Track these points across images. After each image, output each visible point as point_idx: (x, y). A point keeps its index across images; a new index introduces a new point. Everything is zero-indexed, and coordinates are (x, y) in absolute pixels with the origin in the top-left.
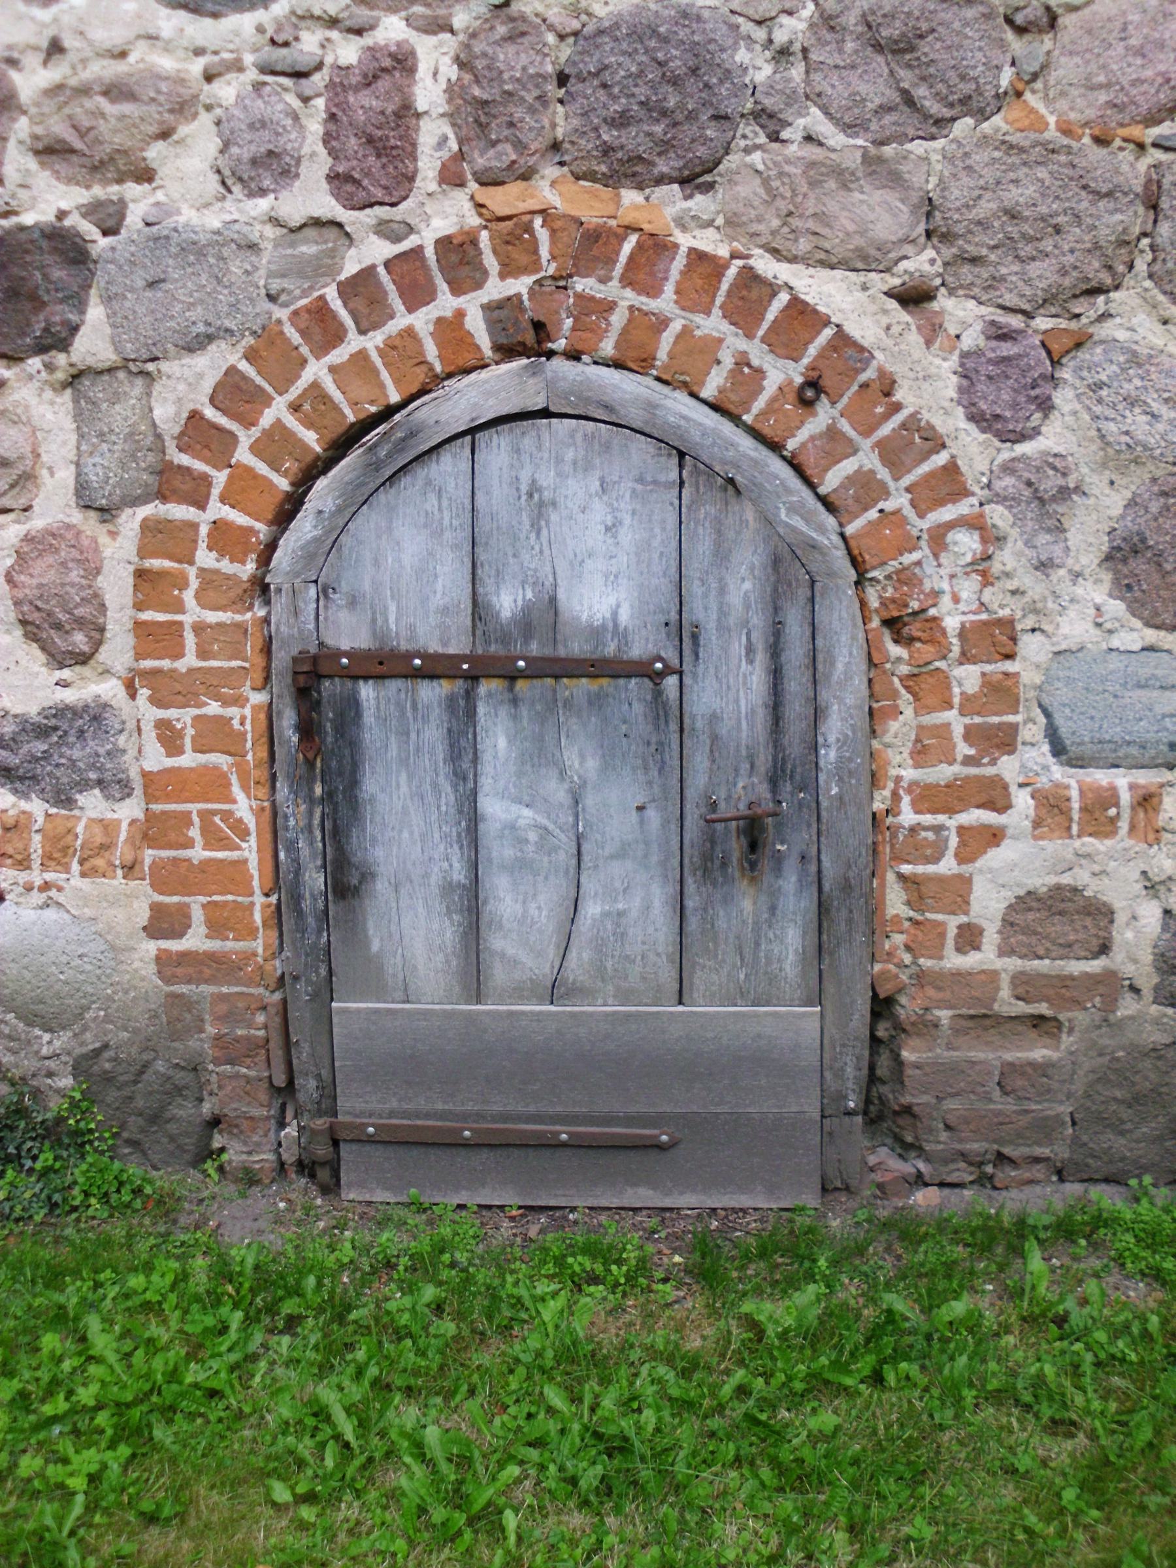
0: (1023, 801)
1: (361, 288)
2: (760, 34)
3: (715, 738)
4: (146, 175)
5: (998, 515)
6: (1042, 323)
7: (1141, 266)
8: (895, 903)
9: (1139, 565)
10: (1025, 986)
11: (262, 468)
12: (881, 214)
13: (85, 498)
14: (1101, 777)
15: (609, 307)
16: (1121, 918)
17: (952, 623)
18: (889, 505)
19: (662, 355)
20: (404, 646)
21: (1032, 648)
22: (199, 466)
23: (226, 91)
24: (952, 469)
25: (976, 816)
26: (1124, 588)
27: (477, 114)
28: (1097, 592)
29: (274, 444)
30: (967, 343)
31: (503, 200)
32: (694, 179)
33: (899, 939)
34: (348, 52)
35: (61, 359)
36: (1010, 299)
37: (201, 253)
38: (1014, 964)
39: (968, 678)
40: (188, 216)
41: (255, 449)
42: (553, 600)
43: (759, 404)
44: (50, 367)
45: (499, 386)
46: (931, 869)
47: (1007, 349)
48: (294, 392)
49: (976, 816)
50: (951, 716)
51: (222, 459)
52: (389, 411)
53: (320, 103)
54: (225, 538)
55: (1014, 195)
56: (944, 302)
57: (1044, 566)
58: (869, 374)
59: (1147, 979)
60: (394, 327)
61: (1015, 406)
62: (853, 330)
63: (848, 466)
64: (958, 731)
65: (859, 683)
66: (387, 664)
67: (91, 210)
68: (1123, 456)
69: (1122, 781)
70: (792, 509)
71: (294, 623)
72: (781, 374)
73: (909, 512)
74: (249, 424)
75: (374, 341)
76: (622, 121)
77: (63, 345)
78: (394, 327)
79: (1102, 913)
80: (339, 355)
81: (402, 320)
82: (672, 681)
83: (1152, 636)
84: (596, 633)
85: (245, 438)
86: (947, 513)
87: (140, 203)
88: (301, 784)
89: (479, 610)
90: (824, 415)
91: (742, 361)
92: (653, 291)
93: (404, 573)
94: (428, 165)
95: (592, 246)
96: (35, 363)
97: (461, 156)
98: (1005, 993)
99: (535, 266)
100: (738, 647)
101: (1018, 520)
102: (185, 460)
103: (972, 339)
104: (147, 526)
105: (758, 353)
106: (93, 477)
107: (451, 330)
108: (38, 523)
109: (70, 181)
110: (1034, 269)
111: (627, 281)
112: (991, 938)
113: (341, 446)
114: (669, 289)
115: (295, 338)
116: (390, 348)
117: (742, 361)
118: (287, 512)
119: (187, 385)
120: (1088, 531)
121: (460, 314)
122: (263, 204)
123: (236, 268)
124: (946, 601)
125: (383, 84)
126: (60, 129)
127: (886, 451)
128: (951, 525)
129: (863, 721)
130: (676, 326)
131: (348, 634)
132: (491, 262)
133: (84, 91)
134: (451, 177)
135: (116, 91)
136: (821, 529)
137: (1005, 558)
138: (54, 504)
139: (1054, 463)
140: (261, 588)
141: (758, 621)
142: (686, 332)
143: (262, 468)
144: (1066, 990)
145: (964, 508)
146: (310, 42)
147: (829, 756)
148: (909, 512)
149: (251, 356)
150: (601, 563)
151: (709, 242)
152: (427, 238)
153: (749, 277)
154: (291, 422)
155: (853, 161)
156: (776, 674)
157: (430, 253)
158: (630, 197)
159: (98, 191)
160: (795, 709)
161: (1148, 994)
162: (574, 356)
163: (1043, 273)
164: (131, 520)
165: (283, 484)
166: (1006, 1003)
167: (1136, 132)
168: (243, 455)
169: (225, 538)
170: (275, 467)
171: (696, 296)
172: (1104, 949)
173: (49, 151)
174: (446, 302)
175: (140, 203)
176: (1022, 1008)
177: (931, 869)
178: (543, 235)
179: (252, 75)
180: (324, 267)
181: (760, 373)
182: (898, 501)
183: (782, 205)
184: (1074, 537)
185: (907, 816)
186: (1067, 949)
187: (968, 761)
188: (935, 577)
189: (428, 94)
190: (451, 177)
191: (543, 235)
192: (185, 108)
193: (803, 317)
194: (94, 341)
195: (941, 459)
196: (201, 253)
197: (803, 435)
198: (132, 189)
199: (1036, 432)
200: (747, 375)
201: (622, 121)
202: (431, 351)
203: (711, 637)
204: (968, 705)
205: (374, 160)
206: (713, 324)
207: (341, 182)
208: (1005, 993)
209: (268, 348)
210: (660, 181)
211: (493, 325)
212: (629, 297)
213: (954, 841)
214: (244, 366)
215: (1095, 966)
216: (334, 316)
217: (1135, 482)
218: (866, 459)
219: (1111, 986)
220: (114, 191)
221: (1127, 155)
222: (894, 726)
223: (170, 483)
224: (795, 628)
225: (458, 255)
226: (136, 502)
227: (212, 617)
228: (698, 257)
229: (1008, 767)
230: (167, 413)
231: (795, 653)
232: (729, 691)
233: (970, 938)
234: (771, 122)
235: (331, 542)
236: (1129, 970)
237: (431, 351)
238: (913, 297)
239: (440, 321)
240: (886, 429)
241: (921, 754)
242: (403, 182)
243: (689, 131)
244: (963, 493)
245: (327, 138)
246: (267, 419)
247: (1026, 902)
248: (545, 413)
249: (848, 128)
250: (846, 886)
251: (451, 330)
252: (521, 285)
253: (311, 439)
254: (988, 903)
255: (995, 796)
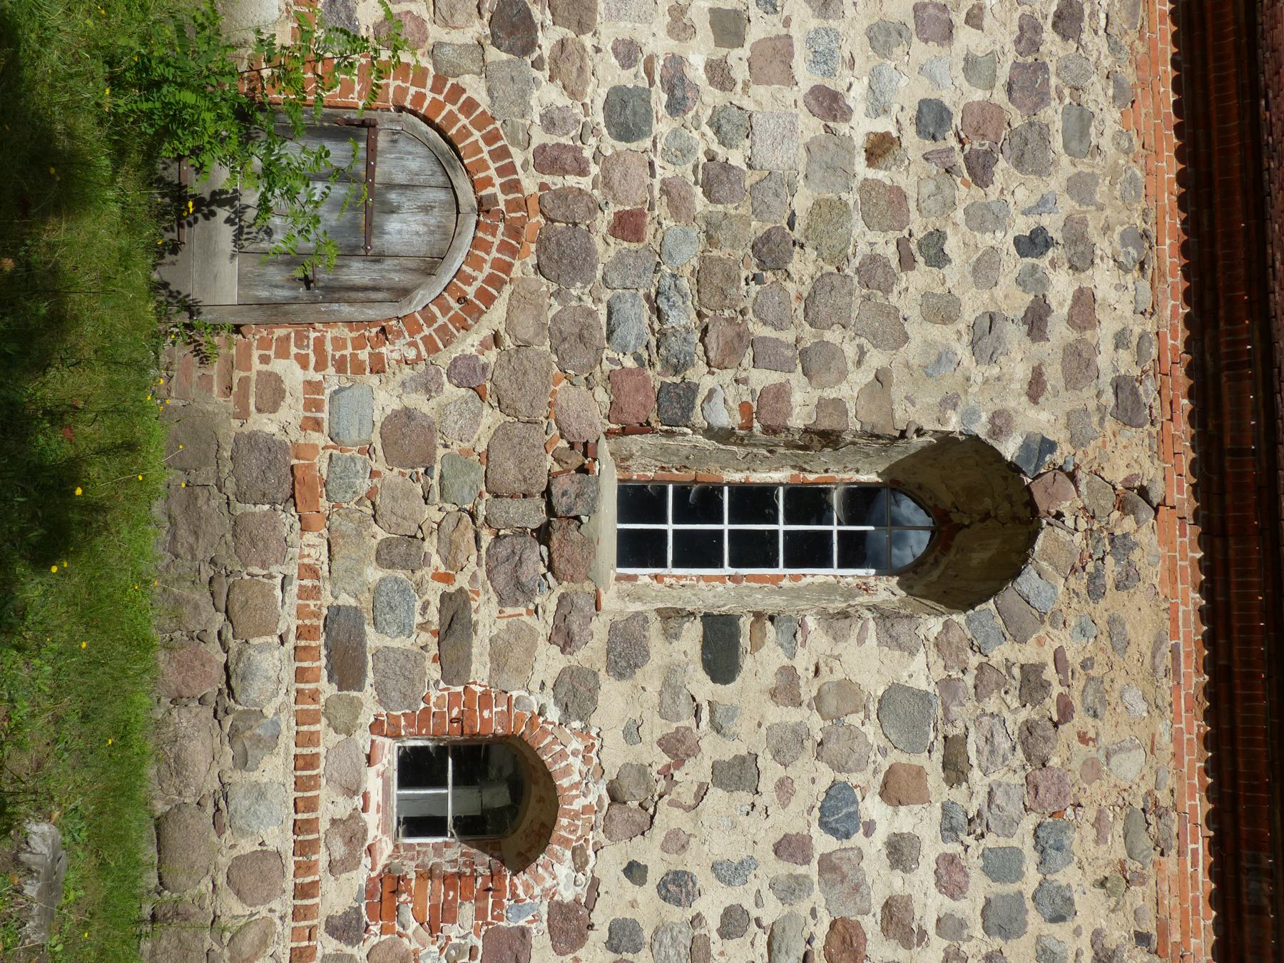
0: (318, 377)
1: (503, 153)
2: (587, 291)
3: (342, 266)
4: (551, 79)
5: (421, 367)
6: (488, 385)
7: (509, 419)
8: (279, 332)
9: (405, 420)
10: (244, 382)
11: (444, 113)
12: (527, 329)
13: (439, 45)
14: (326, 407)
15: (494, 235)
16: (272, 416)
17: (383, 350)
18: (425, 327)
19: (477, 252)
20: (378, 159)
21: (374, 380)
22: (446, 90)
23: (578, 110)
24: (438, 350)
25: (312, 359)
26: (396, 414)
27: (563, 195)
28: (396, 405)
29: (452, 118)
30: (481, 357)
31: (533, 205)
32: (539, 268)
33: (265, 333)
34: (588, 153)
35: (489, 42)
36: (496, 373)
37: (522, 97)
38: (253, 375)
39: (364, 355)
40: (536, 94)
41: (451, 112)
42: (393, 212)
43: (460, 284)
44: (486, 37)
45: (467, 196)
46: (292, 343)
47: (479, 371)
48: (470, 127)
49: (312, 359)
50: (350, 349)
51: (447, 99)
52: (461, 160)
53: (571, 143)
54: (419, 98)
55: (531, 375)
56: (495, 351)
57: (403, 384)
58: (470, 321)
59: (247, 429)
60: (490, 162)
61: (460, 373)
62: (484, 318)
63: (438, 314)
64: (345, 352)
65: (362, 318)
66: (372, 151)
67: (540, 57)
68: (443, 409)
69: (324, 415)
70: (423, 296)
71: (387, 121)
72: (470, 291)
73: (422, 334)
74: (460, 110)
75: (486, 156)
76: (559, 244)
77: (493, 44)
78: (490, 162)
79: (274, 409)
80: (482, 143)
81: (493, 166)
82: (363, 252)
83: (378, 425)
84: (381, 227)
85: (455, 108)
86: (422, 348)
87: (543, 75)
88: (327, 117)
89: (390, 186)
90: (457, 307)
91: (475, 279)
92: (498, 251)
93: (402, 161)
94: (547, 179)
95: (515, 231)
96: (488, 32)
97: (549, 189)
98: (242, 374)
99: (508, 211)
100: (375, 276)
101: (420, 376)
102: (448, 86)
103: (483, 359)
104: (425, 71)
105: (477, 284)
106: (446, 50)
107: (488, 182)
108: (429, 26)
109: (552, 50)
110: (506, 381)
111: (502, 242)
112: (264, 368)
113: (449, 141)
114: (499, 256)
115: (489, 129)
116: (483, 160)
117: (475, 279)
118: (427, 120)
119: (475, 87)
120: (419, 402)
121: (493, 185)
122: (538, 121)
123: (516, 109)
124: (391, 347)
125: (575, 164)
126: (570, 48)
127: (444, 326)
128: (418, 348)
129: (349, 318)
130: (486, 257)
131: (382, 141)
132: (511, 197)
133: (582, 59)
134: (543, 186)
135: (581, 69)
136: (417, 305)
137: (407, 370)
138: (435, 33)
139: (440, 387)
140: (400, 109)
141: (384, 283)
142: (485, 261)
143: (444, 113)
144: (244, 396)
145: (424, 353)
146: (592, 141)
147: (335, 306)
148: (422, 334)
149: (484, 113)
150: (404, 229)
151: (516, 272)
152: (521, 175)
153: (503, 282)
154: (459, 125)
155: (542, 319)
156: (365, 289)
157: (515, 177)
158: (533, 247)
159: (547, 60)
160: (353, 295)
161: (240, 430)
162: (478, 223)
163: (505, 384)
164: (426, 63)
165: (438, 120)
166: (238, 375)
167: (553, 416)
168: (449, 107)
169: (419, 98)
170: (444, 118)
171: (497, 264)
172: (259, 410)
173: (562, 44)
174: (498, 181)
175: (543, 75)
176: (235, 381)
177: (292, 343)
178: (519, 215)
179: (583, 119)
180: (514, 142)
181: (470, 285)
182: (426, 331)
183: (528, 296)
184: (414, 395)
185: (313, 335)
186: (259, 396)
187: (333, 356)
188: (400, 343)
189: (571, 181)
190: (543, 186)
191: (519, 215)
192: (573, 95)
193: (489, 300)
194: (493, 54)
195: (441, 346)
196: (522, 97)
197: (449, 299)
198: (547, 73)
199: (450, 382)
200: (468, 280)
201: (559, 244)
202: (481, 175)
203: (377, 267)
204: (354, 356)
205: (549, 161)
206: (487, 269)
207: (543, 147)
208: (242, 374)
209: (485, 120)
210: (538, 257)
211: (489, 196)
212: (497, 242)
213: (303, 352)
214: (480, 110)
215: (252, 408)
216: (495, 142)
217: (433, 416)
218: (441, 320)
219: (243, 415)
220: (547, 67)
221: (545, 414)
222: (346, 330)
223: (439, 81)
224: (380, 296)
225: (513, 186)
226: (435, 65)
227: (391, 90)
228: (510, 265)
229: (331, 370)
230: (467, 81)
231: (373, 295)
232: (358, 273)
233: (265, 359)
234: (556, 295)
235: (415, 138)
236: (250, 420)
237: (481, 175)
238: (496, 339)
239: (491, 179)
240: (450, 326)
241: (335, 339)
242: (540, 168)
243: (554, 265)
244: (428, 352)
245: (558, 144)
246: (461, 116)
247: (279, 380)
248: (458, 212)
249: (554, 319)
250: (286, 314)
251: (488, 182)
252: (502, 206)
253: (453, 132)
254: (278, 366)
255: (320, 366)
